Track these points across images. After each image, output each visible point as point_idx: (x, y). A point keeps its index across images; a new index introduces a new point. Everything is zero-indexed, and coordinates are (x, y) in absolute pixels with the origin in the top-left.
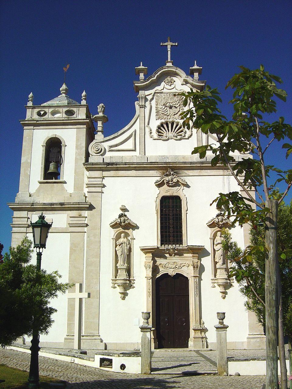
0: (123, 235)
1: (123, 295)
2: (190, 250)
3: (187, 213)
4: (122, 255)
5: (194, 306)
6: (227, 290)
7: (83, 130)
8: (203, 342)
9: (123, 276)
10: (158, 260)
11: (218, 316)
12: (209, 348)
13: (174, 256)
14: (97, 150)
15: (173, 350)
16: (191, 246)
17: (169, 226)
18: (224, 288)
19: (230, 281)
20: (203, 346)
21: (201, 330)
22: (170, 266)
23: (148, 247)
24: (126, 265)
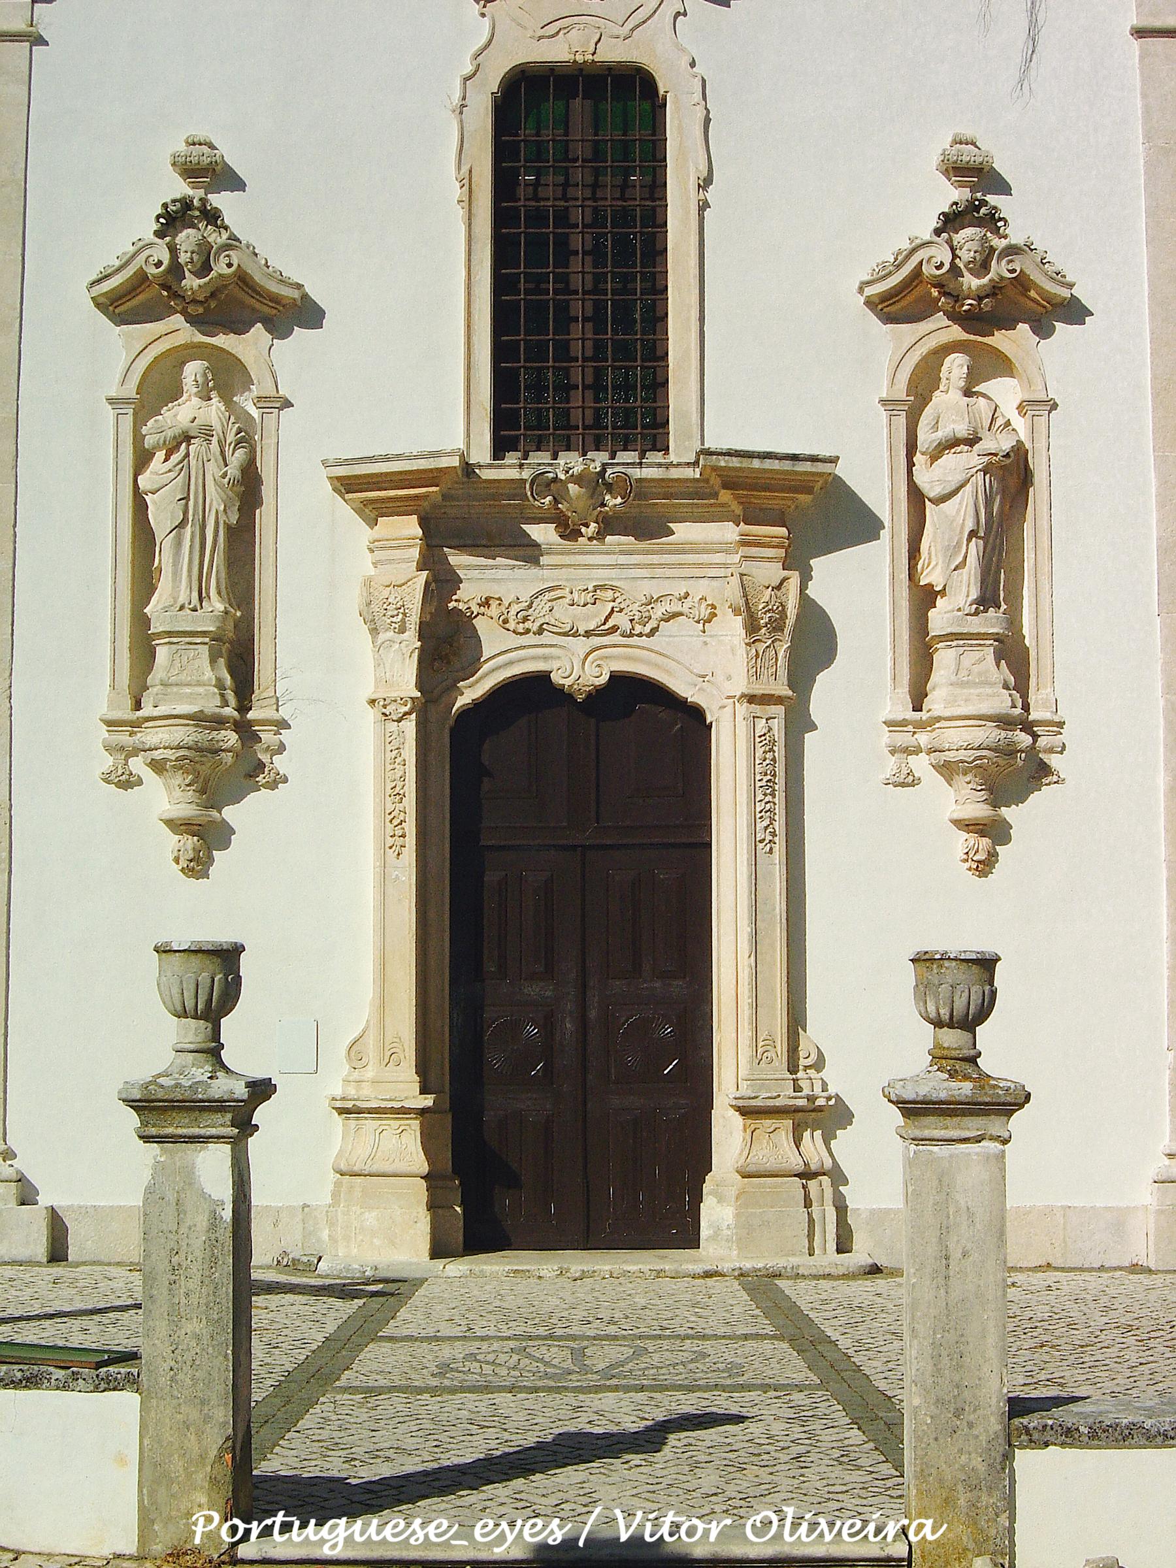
0: (193, 370)
1: (191, 842)
2: (726, 486)
3: (703, 206)
4: (182, 525)
5: (745, 929)
6: (1004, 811)
8: (808, 1203)
9: (188, 690)
10: (468, 567)
11: (923, 989)
12: (859, 1256)
13: (600, 536)
15: (575, 1269)
16: (729, 453)
17: (563, 309)
18: (990, 790)
19: (1035, 736)
20: (811, 1236)
21: (798, 1110)
22: (564, 615)
23: (387, 458)
24: (220, 606)
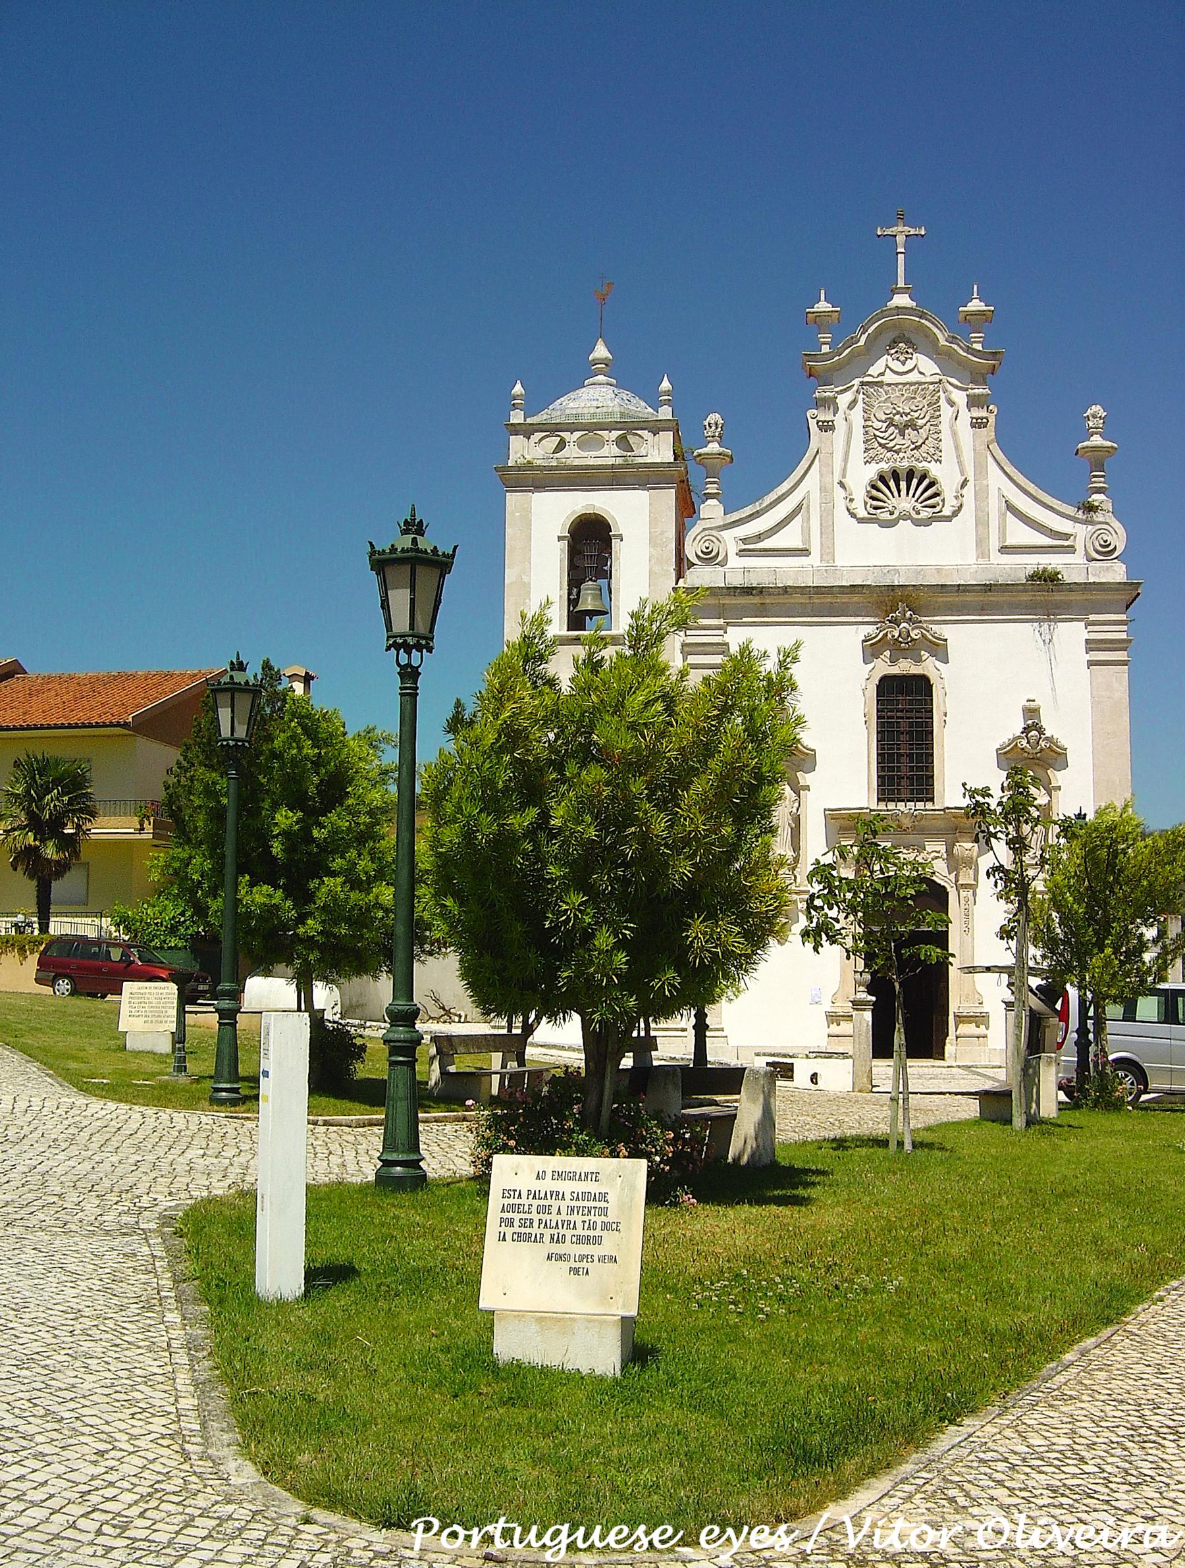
7: (669, 496)
14: (705, 550)
